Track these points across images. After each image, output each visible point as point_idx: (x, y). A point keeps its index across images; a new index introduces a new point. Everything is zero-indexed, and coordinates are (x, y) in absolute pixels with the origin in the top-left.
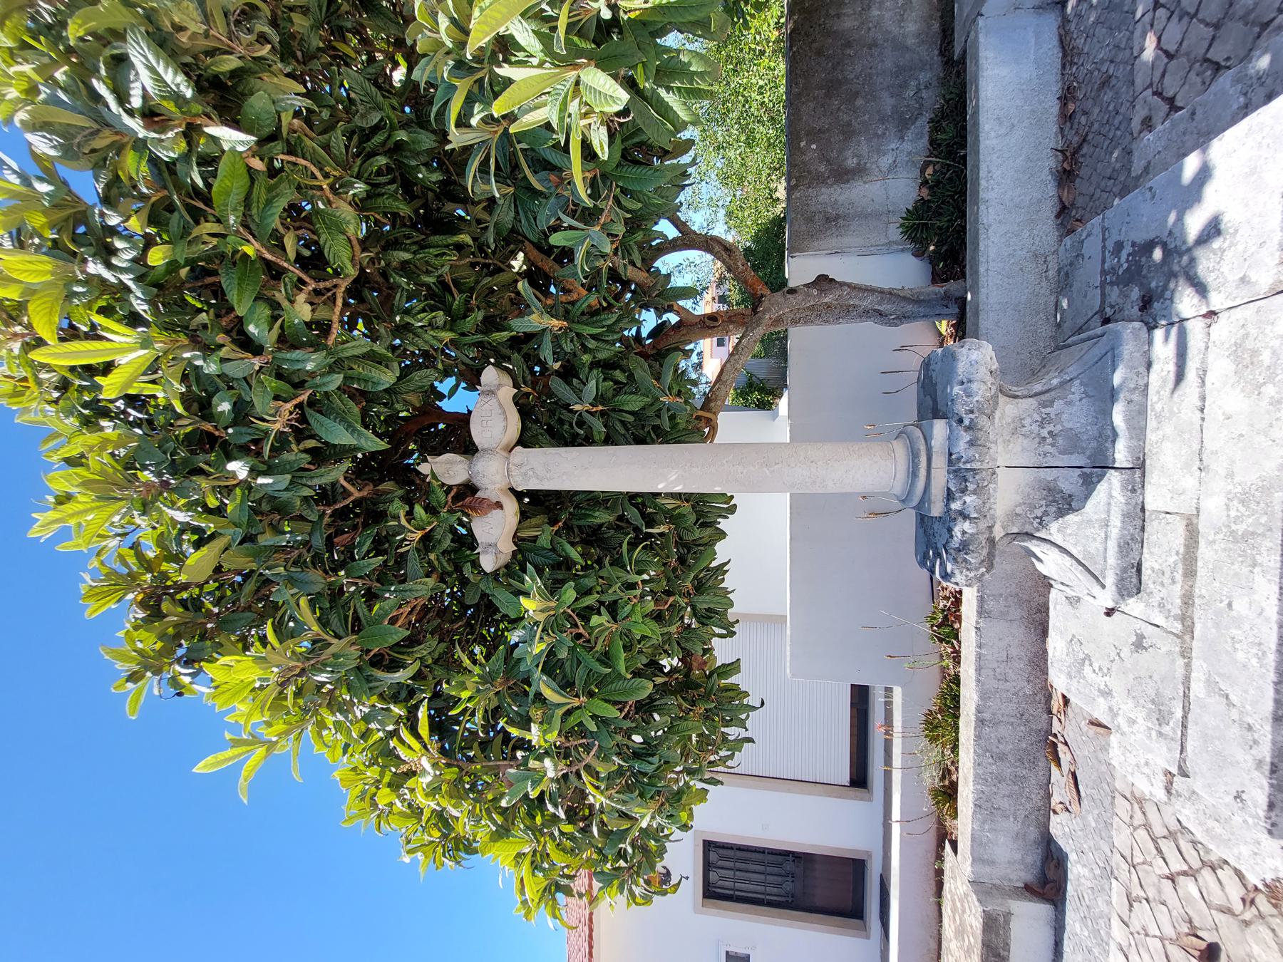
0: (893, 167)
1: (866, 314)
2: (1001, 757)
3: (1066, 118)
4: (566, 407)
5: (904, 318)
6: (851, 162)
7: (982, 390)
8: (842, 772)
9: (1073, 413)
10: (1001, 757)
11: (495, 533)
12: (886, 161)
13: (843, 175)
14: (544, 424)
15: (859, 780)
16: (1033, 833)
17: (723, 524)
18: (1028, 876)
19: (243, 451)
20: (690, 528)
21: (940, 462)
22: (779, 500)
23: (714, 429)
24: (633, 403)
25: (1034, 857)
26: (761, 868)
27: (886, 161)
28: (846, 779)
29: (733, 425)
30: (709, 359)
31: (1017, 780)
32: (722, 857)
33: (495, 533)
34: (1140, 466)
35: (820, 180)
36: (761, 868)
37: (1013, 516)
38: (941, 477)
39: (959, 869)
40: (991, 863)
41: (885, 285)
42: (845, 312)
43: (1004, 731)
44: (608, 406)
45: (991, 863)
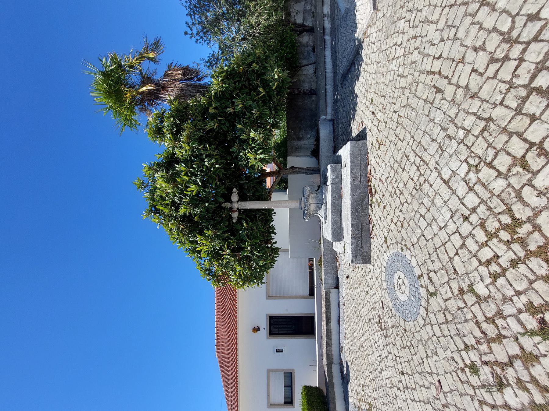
0: (310, 138)
1: (303, 173)
2: (328, 262)
3: (334, 141)
4: (246, 194)
5: (311, 174)
6: (301, 136)
7: (307, 193)
8: (308, 293)
9: (320, 196)
10: (328, 262)
11: (235, 215)
12: (309, 136)
13: (299, 139)
14: (243, 198)
15: (312, 293)
16: (335, 277)
17: (276, 259)
18: (334, 286)
19: (207, 202)
20: (268, 214)
21: (303, 203)
22: (282, 211)
23: (271, 198)
24: (258, 194)
25: (335, 282)
26: (286, 329)
27: (309, 136)
28: (308, 294)
29: (275, 196)
30: (269, 182)
31: (331, 266)
32: (275, 328)
33: (235, 215)
34: (326, 203)
35: (294, 139)
36: (286, 329)
37: (314, 210)
38: (303, 205)
39: (323, 286)
40: (328, 284)
41: (305, 167)
42: (299, 173)
43: (328, 256)
44: (253, 195)
45: (328, 284)
